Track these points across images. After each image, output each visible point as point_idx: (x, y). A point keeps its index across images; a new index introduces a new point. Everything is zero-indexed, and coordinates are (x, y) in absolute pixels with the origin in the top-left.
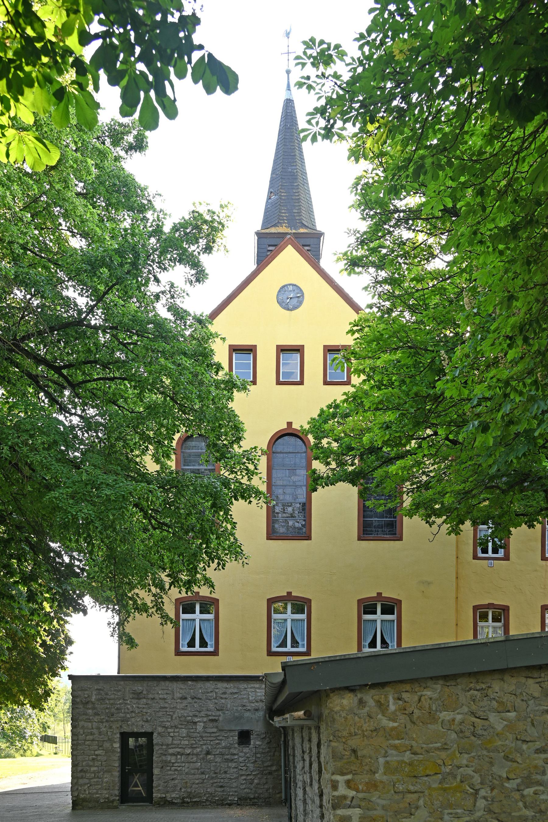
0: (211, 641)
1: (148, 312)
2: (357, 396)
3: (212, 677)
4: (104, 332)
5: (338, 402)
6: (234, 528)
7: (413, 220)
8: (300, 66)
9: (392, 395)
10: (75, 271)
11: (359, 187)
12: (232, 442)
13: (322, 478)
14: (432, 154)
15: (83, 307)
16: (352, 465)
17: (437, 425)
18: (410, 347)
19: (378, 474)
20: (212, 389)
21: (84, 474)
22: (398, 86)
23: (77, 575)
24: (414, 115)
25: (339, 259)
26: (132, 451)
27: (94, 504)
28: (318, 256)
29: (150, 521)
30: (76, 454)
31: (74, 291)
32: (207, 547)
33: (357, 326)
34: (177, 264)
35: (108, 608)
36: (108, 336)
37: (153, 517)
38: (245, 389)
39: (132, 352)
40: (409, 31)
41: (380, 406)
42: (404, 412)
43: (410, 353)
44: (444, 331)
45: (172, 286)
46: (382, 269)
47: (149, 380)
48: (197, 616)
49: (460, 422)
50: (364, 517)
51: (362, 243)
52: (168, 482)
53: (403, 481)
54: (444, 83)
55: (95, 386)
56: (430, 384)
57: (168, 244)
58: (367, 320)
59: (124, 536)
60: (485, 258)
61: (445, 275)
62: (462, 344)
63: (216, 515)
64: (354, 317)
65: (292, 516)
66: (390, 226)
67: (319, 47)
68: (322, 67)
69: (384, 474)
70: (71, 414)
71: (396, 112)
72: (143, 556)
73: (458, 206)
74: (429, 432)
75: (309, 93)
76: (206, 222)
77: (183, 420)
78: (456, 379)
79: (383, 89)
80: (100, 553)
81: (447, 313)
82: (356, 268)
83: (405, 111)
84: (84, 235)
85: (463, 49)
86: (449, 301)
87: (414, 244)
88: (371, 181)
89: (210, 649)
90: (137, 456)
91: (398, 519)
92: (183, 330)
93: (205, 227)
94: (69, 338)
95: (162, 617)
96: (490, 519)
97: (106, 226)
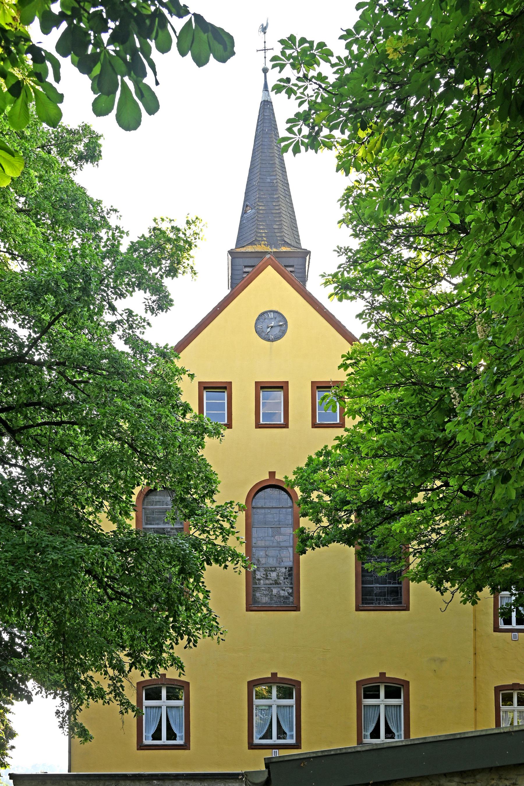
0: (180, 732)
1: (101, 345)
2: (352, 441)
3: (182, 775)
4: (50, 368)
5: (329, 448)
6: (207, 597)
7: (414, 237)
8: (278, 69)
9: (394, 439)
10: (15, 298)
11: (351, 200)
12: (204, 496)
13: (312, 538)
14: (434, 163)
15: (25, 339)
16: (348, 522)
17: (447, 474)
18: (414, 384)
19: (380, 531)
20: (179, 434)
21: (26, 535)
22: (393, 88)
23: (18, 656)
24: (413, 121)
25: (326, 284)
26: (83, 508)
27: (37, 571)
28: (304, 279)
29: (105, 590)
30: (17, 512)
31: (15, 322)
32: (175, 621)
33: (351, 359)
34: (136, 289)
35: (56, 694)
36: (54, 373)
37: (109, 586)
38: (218, 433)
39: (83, 392)
40: (404, 27)
41: (380, 452)
42: (409, 459)
43: (415, 390)
44: (453, 364)
45: (130, 313)
46: (379, 293)
47: (102, 423)
48: (164, 702)
49: (475, 470)
50: (363, 583)
51: (354, 262)
52: (127, 545)
53: (410, 540)
54: (446, 85)
55: (39, 432)
56: (439, 426)
57: (124, 266)
58: (363, 353)
59: (75, 608)
60: (501, 282)
61: (453, 300)
62: (475, 379)
63: (185, 583)
64: (348, 348)
65: (276, 583)
66: (388, 244)
67: (299, 46)
68: (303, 70)
69: (386, 532)
70: (11, 465)
71: (392, 117)
72: (97, 631)
73: (467, 220)
74: (438, 483)
75: (289, 98)
76: (169, 240)
77: (144, 471)
78: (470, 420)
79: (377, 90)
80: (46, 630)
81: (457, 343)
82: (348, 292)
83: (402, 116)
84: (26, 257)
85: (466, 48)
86: (459, 330)
87: (416, 264)
88: (364, 192)
89: (179, 742)
90: (90, 514)
91: (403, 585)
92: (143, 365)
93: (169, 246)
94: (8, 376)
95: (122, 704)
96: (513, 584)
97: (51, 247)
